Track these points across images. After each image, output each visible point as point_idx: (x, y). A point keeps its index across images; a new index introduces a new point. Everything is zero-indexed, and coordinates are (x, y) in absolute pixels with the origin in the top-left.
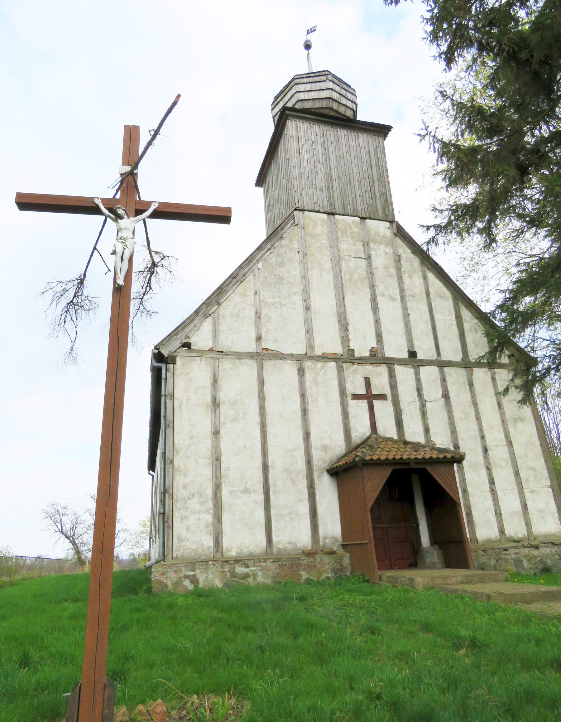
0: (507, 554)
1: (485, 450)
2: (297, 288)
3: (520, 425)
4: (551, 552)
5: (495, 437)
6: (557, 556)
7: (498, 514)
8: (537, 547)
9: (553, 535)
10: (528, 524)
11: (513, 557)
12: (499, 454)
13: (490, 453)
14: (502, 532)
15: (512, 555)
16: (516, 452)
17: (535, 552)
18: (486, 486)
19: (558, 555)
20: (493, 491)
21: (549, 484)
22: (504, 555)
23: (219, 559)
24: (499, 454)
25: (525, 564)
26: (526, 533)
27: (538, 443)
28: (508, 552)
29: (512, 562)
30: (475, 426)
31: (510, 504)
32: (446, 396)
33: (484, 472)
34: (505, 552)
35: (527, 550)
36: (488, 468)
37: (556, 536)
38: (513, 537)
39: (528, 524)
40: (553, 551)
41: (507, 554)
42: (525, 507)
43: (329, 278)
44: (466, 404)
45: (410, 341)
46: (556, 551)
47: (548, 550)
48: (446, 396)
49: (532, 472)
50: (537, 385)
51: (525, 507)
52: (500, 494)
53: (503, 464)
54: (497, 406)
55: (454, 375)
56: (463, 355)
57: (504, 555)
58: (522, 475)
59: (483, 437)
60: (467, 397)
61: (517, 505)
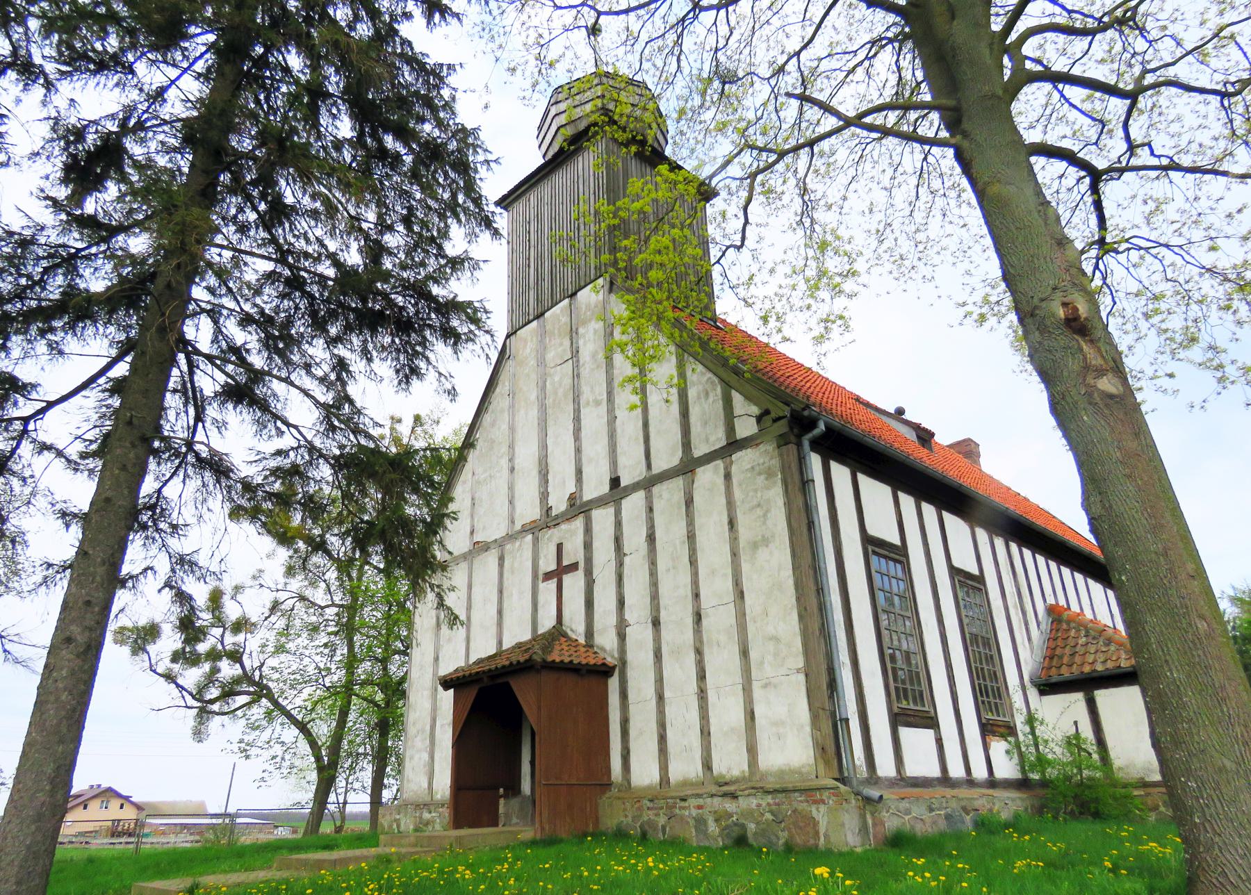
0: (684, 808)
1: (698, 617)
2: (504, 449)
3: (763, 554)
4: (759, 805)
5: (716, 588)
6: (769, 816)
7: (705, 733)
8: (734, 796)
9: (793, 772)
10: (752, 750)
11: (694, 812)
12: (719, 620)
13: (705, 622)
14: (707, 766)
15: (690, 811)
16: (748, 612)
17: (730, 806)
18: (693, 686)
19: (771, 812)
20: (702, 694)
21: (801, 664)
22: (681, 808)
23: (754, 782)
24: (719, 620)
25: (712, 827)
26: (746, 768)
27: (791, 582)
28: (686, 804)
29: (692, 822)
30: (687, 579)
31: (727, 712)
32: (651, 538)
33: (691, 658)
34: (683, 804)
35: (717, 800)
36: (699, 652)
37: (800, 773)
38: (724, 777)
39: (752, 750)
40: (764, 803)
41: (684, 808)
42: (751, 716)
43: (534, 413)
44: (678, 542)
45: (614, 463)
46: (769, 804)
47: (754, 802)
48: (651, 538)
49: (771, 646)
50: (197, 280)
51: (751, 716)
52: (711, 695)
53: (723, 638)
54: (726, 527)
55: (665, 495)
56: (683, 452)
57: (681, 808)
58: (754, 655)
59: (697, 596)
60: (680, 529)
61: (737, 716)
